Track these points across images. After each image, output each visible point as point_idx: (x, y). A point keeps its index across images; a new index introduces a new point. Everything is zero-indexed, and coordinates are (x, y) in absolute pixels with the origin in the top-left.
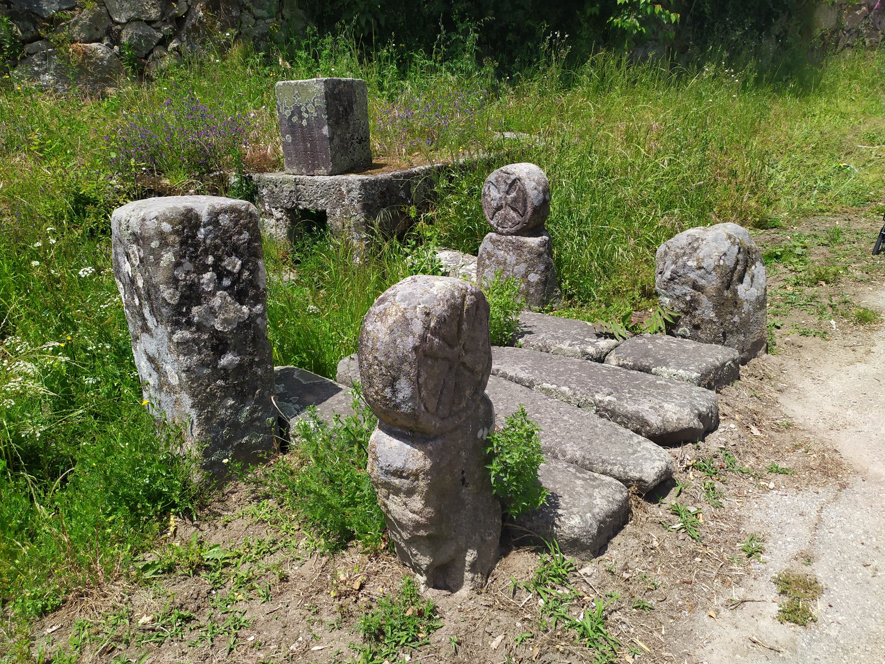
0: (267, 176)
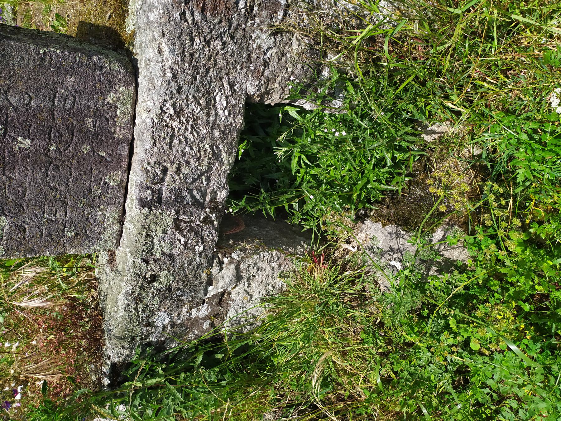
0: (117, 311)
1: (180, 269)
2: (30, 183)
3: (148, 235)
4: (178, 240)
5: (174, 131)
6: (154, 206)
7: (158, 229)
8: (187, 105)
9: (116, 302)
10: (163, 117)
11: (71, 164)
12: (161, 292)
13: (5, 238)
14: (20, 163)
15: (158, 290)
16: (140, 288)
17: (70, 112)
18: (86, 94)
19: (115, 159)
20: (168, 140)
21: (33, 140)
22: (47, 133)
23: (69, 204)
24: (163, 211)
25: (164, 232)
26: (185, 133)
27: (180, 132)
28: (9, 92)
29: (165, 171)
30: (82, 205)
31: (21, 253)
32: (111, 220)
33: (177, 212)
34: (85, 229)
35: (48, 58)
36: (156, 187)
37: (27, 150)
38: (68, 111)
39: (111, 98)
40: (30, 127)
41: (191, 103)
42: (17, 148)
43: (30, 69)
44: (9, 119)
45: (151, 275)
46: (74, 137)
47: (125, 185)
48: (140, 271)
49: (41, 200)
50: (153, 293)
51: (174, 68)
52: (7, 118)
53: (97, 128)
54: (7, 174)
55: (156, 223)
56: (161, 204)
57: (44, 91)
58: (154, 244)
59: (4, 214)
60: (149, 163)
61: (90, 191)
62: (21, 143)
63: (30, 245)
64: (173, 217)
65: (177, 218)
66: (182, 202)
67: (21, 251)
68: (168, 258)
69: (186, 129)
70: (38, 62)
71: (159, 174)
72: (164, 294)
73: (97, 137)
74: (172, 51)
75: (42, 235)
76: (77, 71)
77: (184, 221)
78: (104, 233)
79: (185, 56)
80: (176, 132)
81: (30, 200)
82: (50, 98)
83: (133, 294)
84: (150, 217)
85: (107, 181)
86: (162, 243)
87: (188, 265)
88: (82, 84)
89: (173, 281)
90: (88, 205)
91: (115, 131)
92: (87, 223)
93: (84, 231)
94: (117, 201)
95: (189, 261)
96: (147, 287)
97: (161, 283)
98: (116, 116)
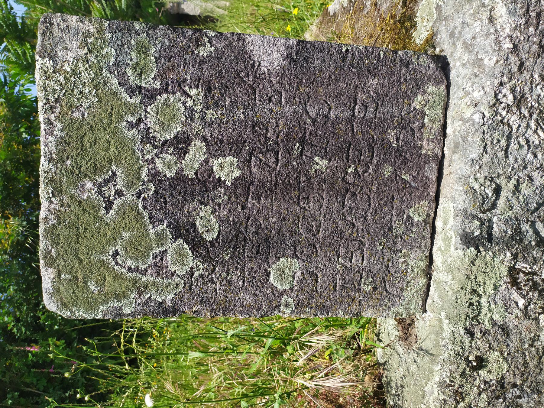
1: (518, 351)
2: (325, 216)
3: (474, 291)
4: (515, 302)
5: (512, 129)
6: (483, 245)
7: (487, 283)
8: (531, 89)
9: (424, 397)
10: (497, 110)
11: (370, 191)
12: (490, 386)
13: (296, 288)
14: (315, 190)
15: (486, 382)
16: (461, 376)
17: (371, 124)
18: (390, 98)
19: (421, 184)
20: (503, 142)
21: (330, 160)
22: (344, 152)
23: (367, 246)
24: (494, 254)
25: (496, 288)
26: (526, 132)
27: (520, 131)
28: (308, 101)
29: (498, 191)
30: (381, 247)
31: (313, 311)
32: (415, 270)
33: (515, 257)
34: (385, 282)
35: (350, 57)
36: (484, 217)
37: (324, 173)
38: (369, 121)
39: (418, 102)
40: (327, 144)
41: (536, 87)
42: (313, 171)
43: (331, 71)
44: (307, 135)
45: (476, 357)
46: (375, 155)
47: (431, 221)
48: (462, 348)
49: (337, 239)
50: (479, 387)
51: (514, 36)
52: (305, 133)
53: (400, 142)
54: (301, 203)
55: (485, 273)
56: (491, 243)
57: (344, 99)
58: (481, 306)
59: (296, 256)
60: (476, 180)
61: (390, 229)
62: (317, 164)
63: (322, 300)
64: (508, 264)
65: (514, 265)
66: (521, 240)
67: (312, 308)
68: (500, 330)
69: (528, 126)
70: (339, 63)
71: (490, 195)
72: (494, 390)
73: (401, 155)
74: (511, 12)
75: (336, 286)
76: (380, 71)
77: (524, 272)
78: (407, 290)
79: (530, 16)
80: (515, 130)
81: (324, 238)
82: (350, 106)
83: (450, 385)
84: (477, 262)
85: (412, 215)
86: (493, 305)
87: (529, 345)
88: (386, 87)
89: (508, 371)
90: (389, 248)
91: (421, 145)
92: (387, 272)
93: (383, 285)
94: (423, 242)
95: (530, 338)
96: (470, 376)
97: (489, 372)
98: (423, 125)
